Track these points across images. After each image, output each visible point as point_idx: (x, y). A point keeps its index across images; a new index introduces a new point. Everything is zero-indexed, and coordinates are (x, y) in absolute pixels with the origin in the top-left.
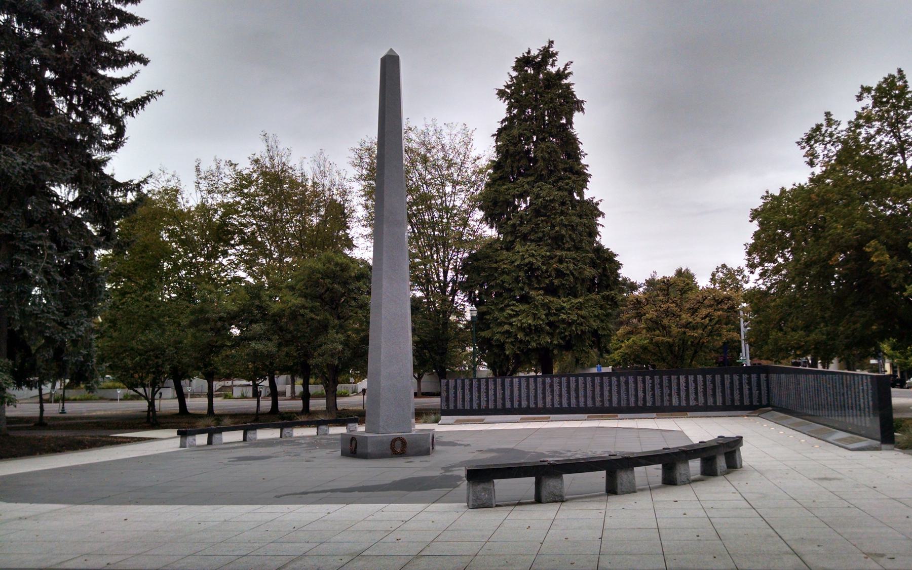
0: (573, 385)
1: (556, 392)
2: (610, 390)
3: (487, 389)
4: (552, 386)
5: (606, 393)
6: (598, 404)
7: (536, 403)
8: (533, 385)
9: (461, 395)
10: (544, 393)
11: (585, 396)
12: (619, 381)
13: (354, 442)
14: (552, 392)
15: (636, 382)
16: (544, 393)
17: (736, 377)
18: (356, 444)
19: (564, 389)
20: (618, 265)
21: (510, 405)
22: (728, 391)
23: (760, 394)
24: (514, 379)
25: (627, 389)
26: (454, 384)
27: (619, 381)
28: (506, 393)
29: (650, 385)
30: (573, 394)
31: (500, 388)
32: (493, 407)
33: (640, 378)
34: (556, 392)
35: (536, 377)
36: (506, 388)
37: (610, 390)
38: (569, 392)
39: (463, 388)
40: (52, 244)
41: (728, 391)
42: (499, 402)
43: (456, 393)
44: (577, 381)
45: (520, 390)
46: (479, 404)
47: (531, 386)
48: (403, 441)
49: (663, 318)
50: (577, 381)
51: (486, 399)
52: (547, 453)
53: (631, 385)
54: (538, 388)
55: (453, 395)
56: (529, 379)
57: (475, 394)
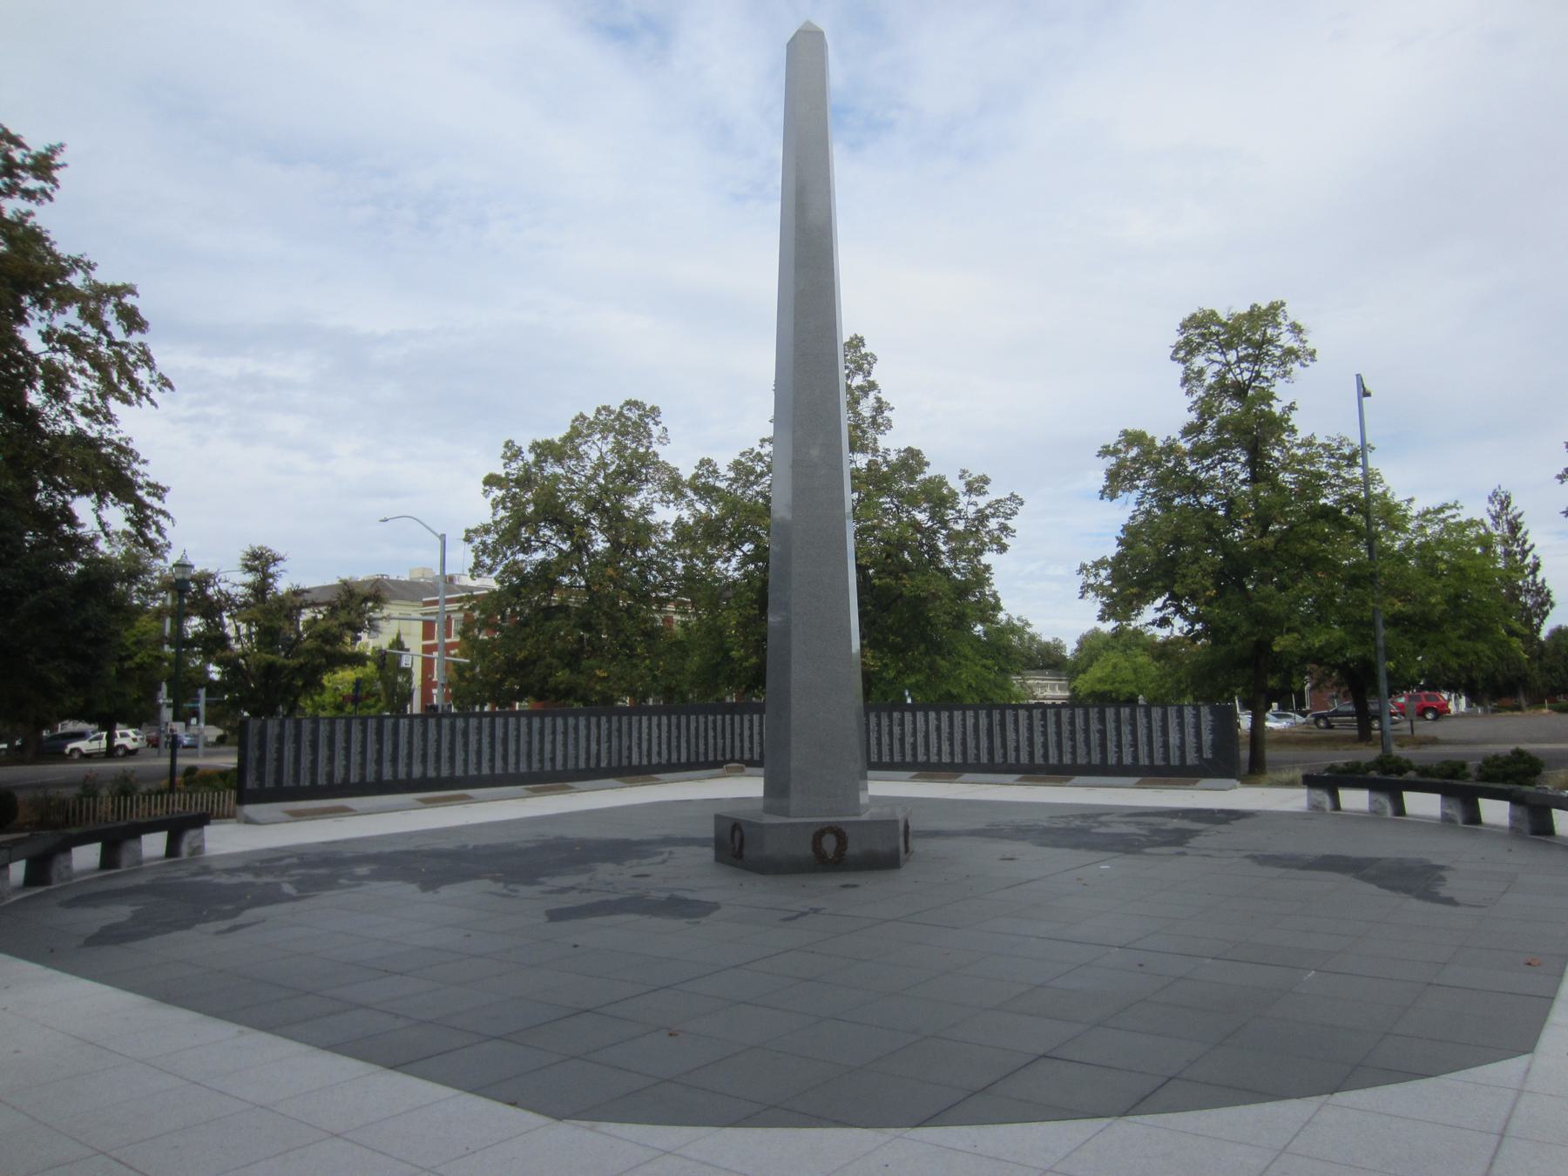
0: (499, 733)
1: (473, 746)
2: (554, 742)
3: (348, 741)
4: (465, 734)
5: (548, 747)
6: (1053, 760)
7: (1046, 756)
8: (435, 732)
9: (292, 754)
10: (452, 749)
11: (1135, 744)
12: (566, 724)
13: (737, 835)
14: (466, 744)
15: (588, 727)
16: (452, 749)
17: (571, 721)
18: (742, 840)
19: (486, 740)
20: (77, 518)
21: (390, 773)
22: (693, 741)
23: (724, 743)
24: (402, 721)
25: (577, 739)
26: (277, 730)
27: (566, 724)
28: (385, 749)
29: (606, 732)
30: (499, 748)
31: (374, 737)
32: (1114, 762)
33: (593, 720)
34: (473, 746)
35: (492, 715)
36: (385, 738)
37: (554, 742)
38: (1073, 738)
39: (298, 739)
40: (131, 477)
41: (693, 741)
42: (371, 769)
43: (280, 751)
44: (506, 725)
45: (410, 743)
46: (330, 775)
47: (430, 735)
48: (839, 833)
49: (349, 613)
50: (506, 725)
51: (344, 763)
52: (365, 882)
53: (582, 732)
54: (443, 740)
55: (275, 756)
56: (367, 721)
57: (323, 752)
